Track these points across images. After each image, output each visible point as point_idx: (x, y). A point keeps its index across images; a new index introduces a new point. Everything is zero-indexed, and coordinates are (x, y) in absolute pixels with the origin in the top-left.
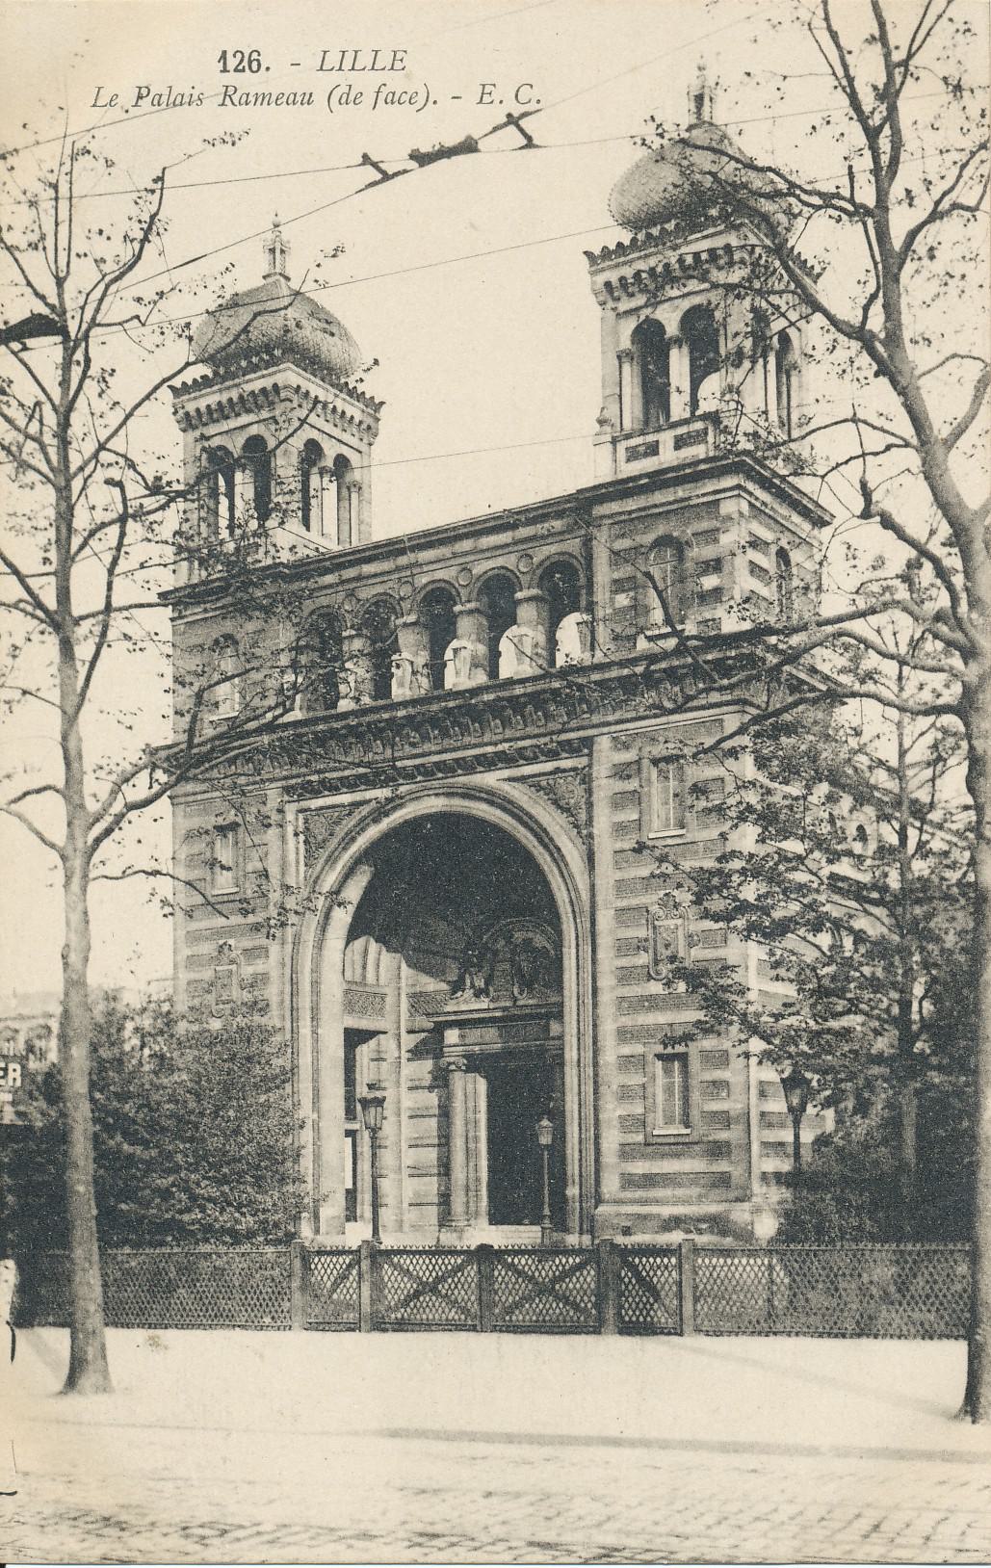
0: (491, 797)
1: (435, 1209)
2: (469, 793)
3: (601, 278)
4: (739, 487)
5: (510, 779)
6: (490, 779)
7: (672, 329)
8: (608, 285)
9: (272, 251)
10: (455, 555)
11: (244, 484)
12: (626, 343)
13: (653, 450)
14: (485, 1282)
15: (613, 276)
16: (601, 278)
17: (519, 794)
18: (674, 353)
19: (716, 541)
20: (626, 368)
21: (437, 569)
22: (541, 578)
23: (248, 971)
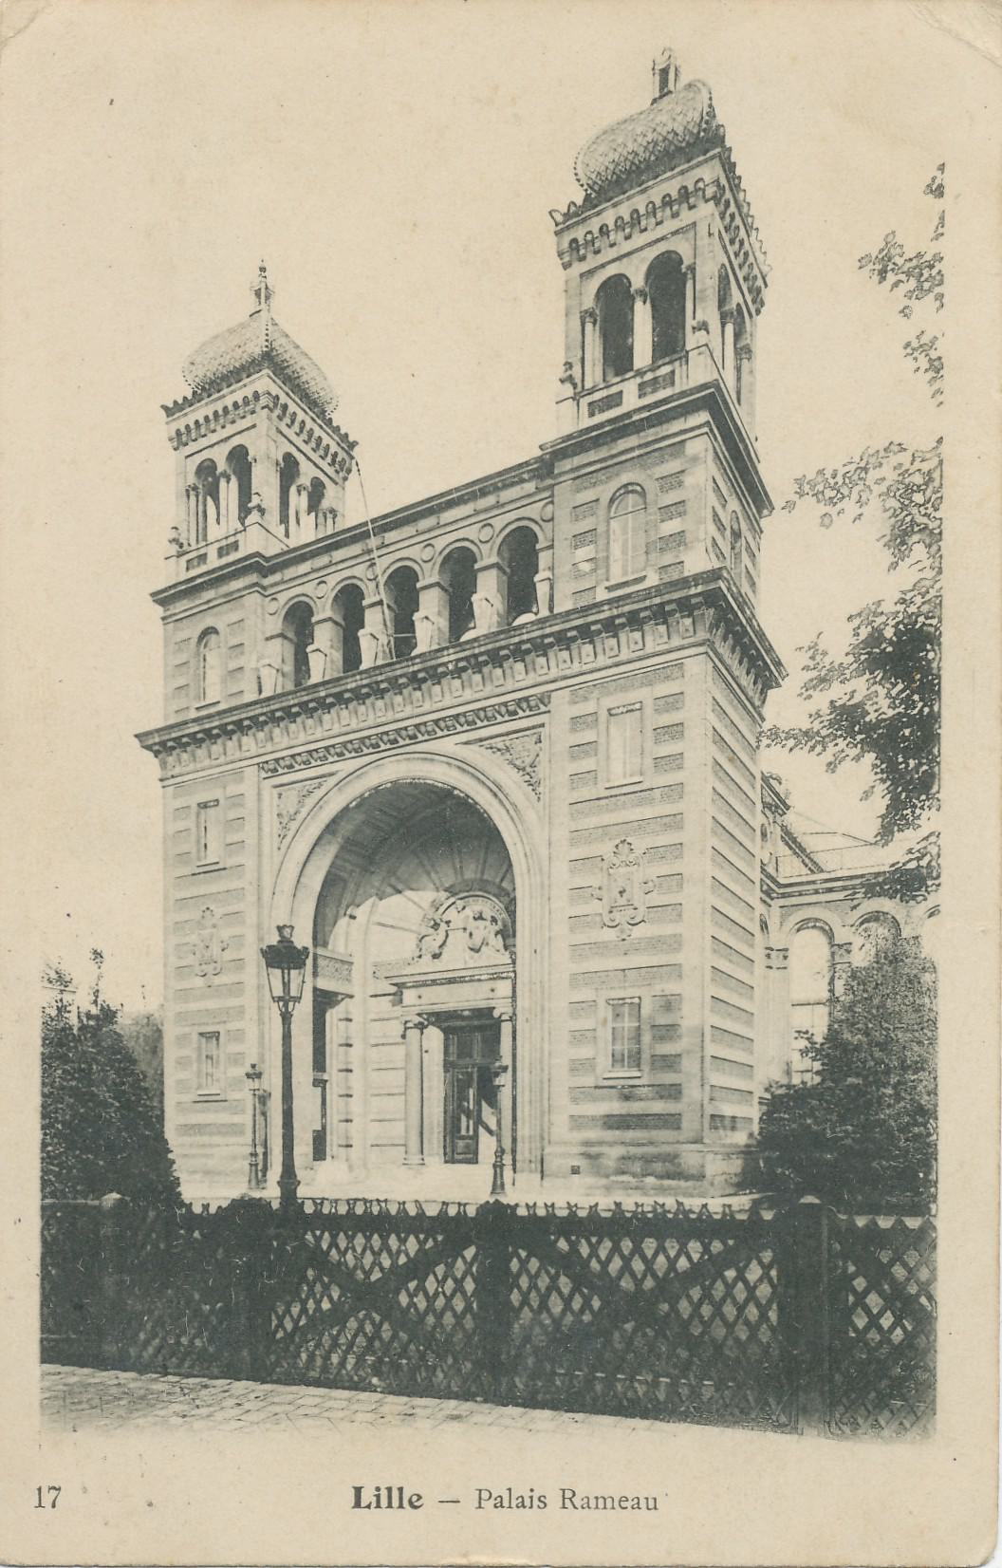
0: (450, 760)
1: (485, 1196)
2: (430, 757)
3: (174, 426)
4: (256, 584)
5: (466, 743)
6: (448, 745)
7: (638, 281)
8: (178, 433)
9: (258, 293)
10: (477, 512)
11: (229, 491)
12: (589, 302)
13: (615, 400)
14: (495, 1281)
15: (181, 425)
16: (174, 426)
17: (475, 755)
18: (638, 305)
19: (680, 484)
20: (589, 327)
21: (463, 528)
22: (443, 564)
23: (226, 933)
